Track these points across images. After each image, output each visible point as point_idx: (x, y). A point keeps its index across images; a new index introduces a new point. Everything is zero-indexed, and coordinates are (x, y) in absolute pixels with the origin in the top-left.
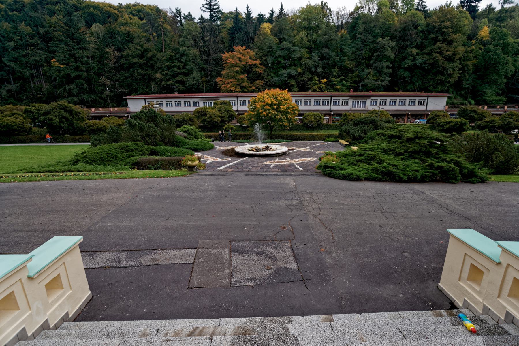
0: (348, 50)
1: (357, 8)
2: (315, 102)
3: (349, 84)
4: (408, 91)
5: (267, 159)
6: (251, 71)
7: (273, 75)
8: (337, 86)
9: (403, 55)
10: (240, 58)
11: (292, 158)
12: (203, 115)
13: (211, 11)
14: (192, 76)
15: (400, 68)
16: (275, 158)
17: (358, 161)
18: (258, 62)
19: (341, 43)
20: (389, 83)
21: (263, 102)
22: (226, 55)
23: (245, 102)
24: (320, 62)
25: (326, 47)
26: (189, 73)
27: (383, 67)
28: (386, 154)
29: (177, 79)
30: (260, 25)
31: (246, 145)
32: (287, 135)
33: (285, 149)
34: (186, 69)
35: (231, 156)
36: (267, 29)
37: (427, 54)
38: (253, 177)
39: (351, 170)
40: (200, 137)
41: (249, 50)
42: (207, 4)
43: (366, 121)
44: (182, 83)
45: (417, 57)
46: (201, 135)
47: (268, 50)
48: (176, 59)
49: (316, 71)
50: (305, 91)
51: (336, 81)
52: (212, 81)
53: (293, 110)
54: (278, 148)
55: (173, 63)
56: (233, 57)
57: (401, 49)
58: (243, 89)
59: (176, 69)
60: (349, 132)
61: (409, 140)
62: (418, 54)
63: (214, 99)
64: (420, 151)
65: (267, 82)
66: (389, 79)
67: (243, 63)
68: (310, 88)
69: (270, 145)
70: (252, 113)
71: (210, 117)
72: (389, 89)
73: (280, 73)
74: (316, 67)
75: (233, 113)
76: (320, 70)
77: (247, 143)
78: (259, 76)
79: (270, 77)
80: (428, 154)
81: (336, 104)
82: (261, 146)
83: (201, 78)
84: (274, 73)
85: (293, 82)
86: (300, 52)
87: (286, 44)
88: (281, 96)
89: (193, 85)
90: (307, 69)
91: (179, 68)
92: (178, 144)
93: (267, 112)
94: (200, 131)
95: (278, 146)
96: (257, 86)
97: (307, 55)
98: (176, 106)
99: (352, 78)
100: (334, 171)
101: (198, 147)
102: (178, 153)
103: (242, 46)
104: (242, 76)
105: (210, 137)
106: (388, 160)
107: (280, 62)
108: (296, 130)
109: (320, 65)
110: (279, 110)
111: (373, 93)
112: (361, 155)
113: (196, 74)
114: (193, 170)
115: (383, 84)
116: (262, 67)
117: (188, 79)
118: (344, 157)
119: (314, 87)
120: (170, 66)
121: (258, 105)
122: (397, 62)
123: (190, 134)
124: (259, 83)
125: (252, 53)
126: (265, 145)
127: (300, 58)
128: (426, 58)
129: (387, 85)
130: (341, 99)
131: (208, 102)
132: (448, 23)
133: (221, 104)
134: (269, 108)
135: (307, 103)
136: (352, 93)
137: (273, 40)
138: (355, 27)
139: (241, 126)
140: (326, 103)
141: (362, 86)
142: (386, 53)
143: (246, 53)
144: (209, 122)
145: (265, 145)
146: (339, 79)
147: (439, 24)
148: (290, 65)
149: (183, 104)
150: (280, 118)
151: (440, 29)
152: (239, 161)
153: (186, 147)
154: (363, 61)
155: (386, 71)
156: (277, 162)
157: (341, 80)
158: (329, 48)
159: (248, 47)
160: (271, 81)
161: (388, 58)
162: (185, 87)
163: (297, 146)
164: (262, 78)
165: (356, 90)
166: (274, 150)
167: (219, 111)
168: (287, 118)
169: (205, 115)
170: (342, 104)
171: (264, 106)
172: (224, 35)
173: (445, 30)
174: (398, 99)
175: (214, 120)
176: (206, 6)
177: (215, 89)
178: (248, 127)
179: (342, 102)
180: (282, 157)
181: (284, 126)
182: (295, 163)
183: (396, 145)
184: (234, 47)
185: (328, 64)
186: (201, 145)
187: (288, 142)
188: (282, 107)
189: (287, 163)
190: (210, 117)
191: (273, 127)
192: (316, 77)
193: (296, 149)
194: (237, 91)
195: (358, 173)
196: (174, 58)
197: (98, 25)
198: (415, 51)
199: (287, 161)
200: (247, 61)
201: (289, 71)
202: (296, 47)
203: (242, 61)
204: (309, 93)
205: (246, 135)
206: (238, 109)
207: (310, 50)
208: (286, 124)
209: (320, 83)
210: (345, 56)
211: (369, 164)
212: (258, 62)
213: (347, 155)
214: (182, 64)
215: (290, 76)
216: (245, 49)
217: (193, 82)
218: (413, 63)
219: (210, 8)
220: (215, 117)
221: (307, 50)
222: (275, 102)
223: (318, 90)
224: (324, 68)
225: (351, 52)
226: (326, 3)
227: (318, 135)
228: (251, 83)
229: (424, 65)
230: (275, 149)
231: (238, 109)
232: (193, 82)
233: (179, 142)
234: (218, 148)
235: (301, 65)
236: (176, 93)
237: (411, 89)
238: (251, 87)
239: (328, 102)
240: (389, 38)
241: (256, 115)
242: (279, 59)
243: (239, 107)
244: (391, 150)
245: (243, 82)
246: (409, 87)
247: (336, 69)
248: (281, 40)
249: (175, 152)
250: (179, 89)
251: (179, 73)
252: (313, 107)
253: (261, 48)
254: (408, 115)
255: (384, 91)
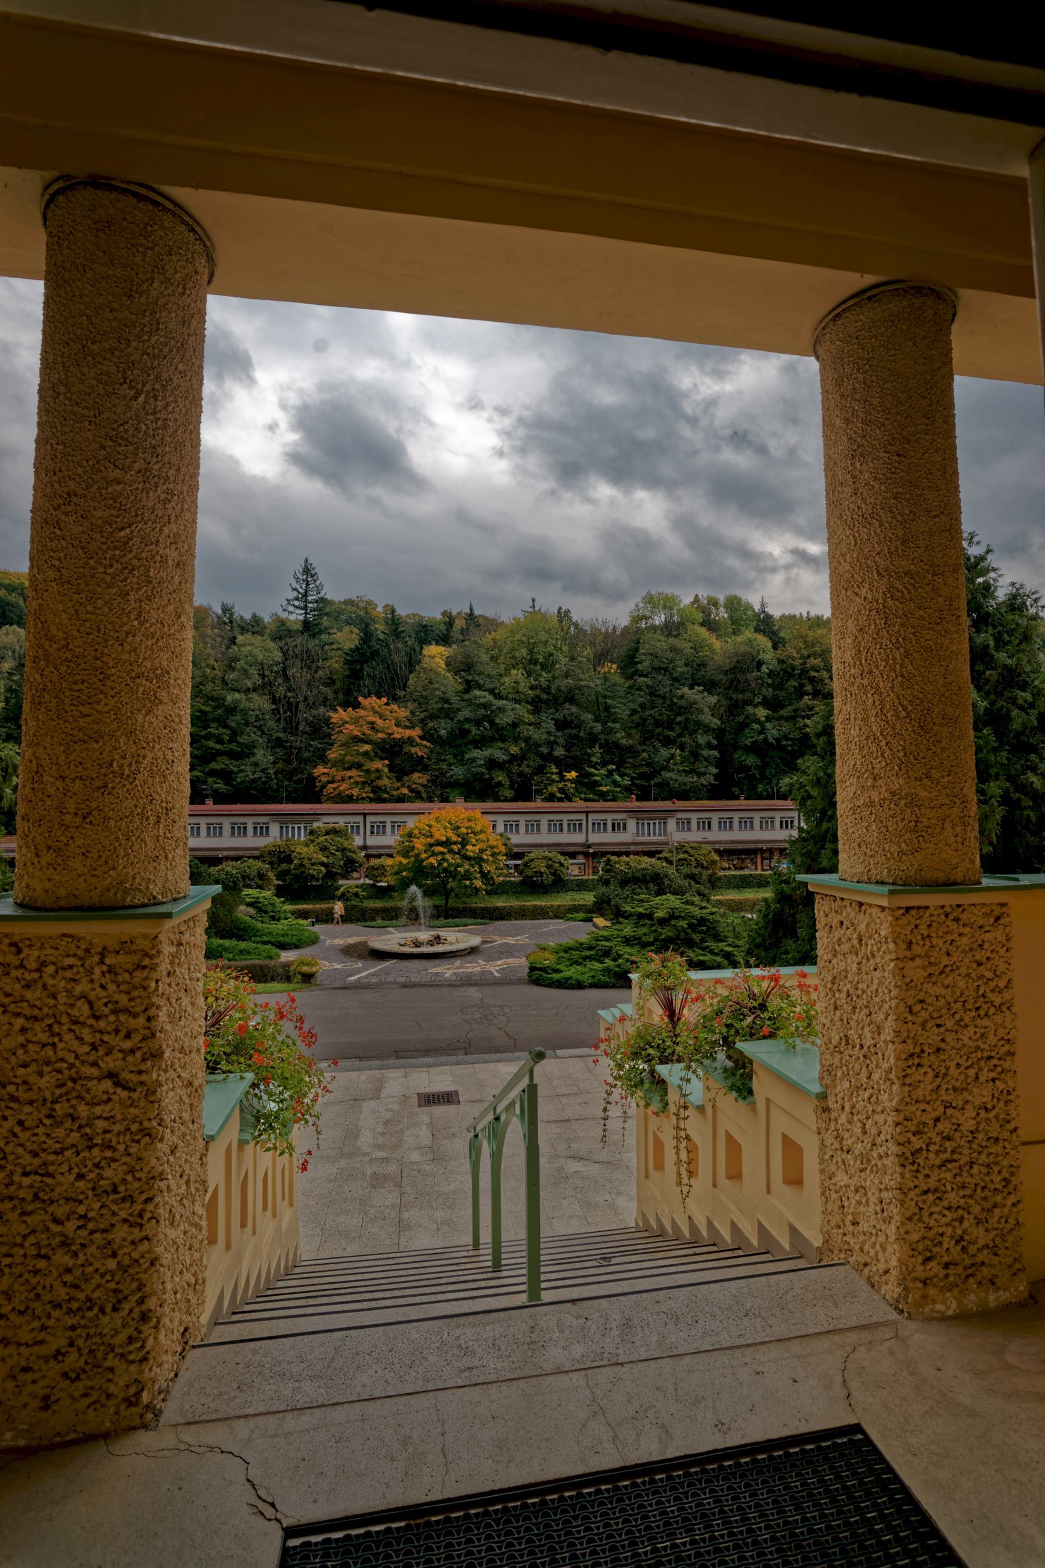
0: (622, 711)
1: (637, 619)
2: (549, 825)
3: (627, 782)
4: (760, 797)
5: (437, 962)
6: (400, 752)
7: (450, 758)
8: (601, 785)
9: (741, 718)
10: (372, 723)
11: (489, 959)
12: (281, 861)
13: (306, 614)
14: (252, 759)
15: (736, 747)
16: (453, 960)
17: (585, 958)
18: (416, 733)
19: (606, 693)
20: (715, 780)
21: (428, 837)
22: (340, 715)
23: (384, 827)
24: (559, 734)
25: (572, 700)
26: (243, 753)
27: (698, 746)
28: (628, 945)
29: (214, 765)
30: (422, 648)
31: (392, 933)
32: (483, 909)
33: (475, 941)
34: (237, 742)
35: (361, 957)
36: (437, 660)
37: (787, 719)
38: (414, 989)
39: (572, 972)
40: (282, 915)
41: (395, 707)
42: (297, 599)
43: (644, 876)
44: (225, 775)
45: (768, 725)
46: (285, 912)
47: (440, 706)
48: (214, 720)
49: (550, 754)
50: (527, 798)
51: (598, 774)
52: (302, 772)
53: (493, 855)
54: (456, 938)
55: (205, 728)
56: (356, 721)
57: (735, 708)
58: (379, 795)
59: (211, 744)
60: (610, 900)
61: (662, 922)
62: (768, 719)
63: (308, 818)
64: (678, 938)
65: (437, 777)
66: (715, 771)
67: (381, 735)
68: (539, 792)
69: (443, 933)
70: (405, 861)
71: (302, 865)
72: (722, 790)
73: (467, 756)
74: (551, 744)
75: (354, 856)
76: (559, 752)
77: (391, 929)
78: (419, 764)
79: (444, 766)
80: (690, 944)
81: (599, 829)
82: (424, 935)
83: (274, 763)
84: (455, 756)
85: (500, 777)
86: (511, 712)
87: (480, 695)
88: (467, 824)
89: (254, 781)
90: (532, 745)
91: (220, 741)
92: (241, 933)
93: (440, 858)
94: (283, 902)
95: (460, 935)
96: (414, 786)
97: (531, 718)
98: (208, 834)
99: (635, 767)
100: (545, 975)
101: (287, 940)
102: (249, 953)
103: (379, 698)
104: (378, 764)
105: (303, 915)
106: (629, 954)
107: (469, 731)
108: (507, 893)
109: (561, 741)
110: (463, 852)
111: (680, 804)
112: (590, 948)
113: (263, 756)
114: (309, 982)
115: (703, 781)
116: (425, 742)
117: (242, 768)
118: (566, 951)
119: (550, 788)
120: (198, 735)
121: (419, 844)
122: (730, 733)
123: (261, 911)
124: (418, 778)
125: (403, 713)
126: (434, 933)
127: (515, 725)
128: (786, 727)
129: (710, 784)
130: (609, 818)
131: (290, 826)
132: (816, 661)
133: (327, 833)
134: (441, 849)
135: (534, 828)
136: (634, 804)
137: (451, 684)
138: (633, 657)
139: (373, 886)
140: (575, 827)
141: (657, 785)
142: (701, 717)
143: (388, 713)
144: (296, 877)
145: (434, 933)
146: (603, 771)
147: (801, 661)
148: (492, 739)
149: (227, 829)
150: (467, 871)
151: (804, 672)
152: (379, 967)
153: (258, 939)
154: (658, 730)
155: (705, 753)
156: (458, 968)
157: (610, 773)
158: (577, 704)
159: (394, 698)
160: (448, 775)
161: (707, 729)
162: (231, 785)
163: (503, 934)
164: (425, 769)
165: (643, 797)
166: (451, 943)
167: (321, 850)
168: (481, 872)
169: (288, 859)
170: (614, 829)
171: (431, 845)
172: (335, 665)
173: (813, 674)
174: (736, 817)
175: (311, 871)
176: (296, 603)
177: (310, 792)
178: (390, 888)
179: (613, 824)
180: (469, 958)
181: (476, 888)
182: (492, 969)
183: (643, 930)
184: (361, 699)
185: (577, 737)
186: (293, 935)
187: (484, 924)
188: (469, 847)
189: (478, 969)
190: (302, 865)
191: (452, 890)
192: (553, 766)
193: (499, 940)
194: (363, 798)
195: (579, 977)
196: (210, 716)
197: (14, 631)
198: (762, 713)
199: (474, 967)
200: (390, 731)
201: (487, 752)
202: (504, 702)
203: (378, 731)
204: (538, 804)
205: (388, 909)
206: (365, 843)
207: (537, 705)
208: (478, 883)
209: (562, 778)
210: (614, 721)
211: (602, 962)
212: (416, 733)
213: (570, 948)
214: (228, 732)
215: (492, 764)
216: (387, 704)
217: (254, 773)
218: (762, 737)
219: (306, 608)
220: (313, 864)
221: (530, 707)
222: (454, 838)
223: (559, 795)
224: (568, 747)
225: (628, 712)
226: (568, 612)
227: (552, 906)
228: (399, 779)
229: (784, 743)
230: (454, 941)
231: (365, 843)
232: (254, 773)
233: (244, 930)
234: (328, 942)
235: (516, 740)
236: (209, 802)
237: (765, 793)
238: (398, 789)
239: (580, 825)
240: (701, 688)
241: (414, 865)
242: (467, 726)
243: (368, 838)
244: (636, 939)
245: (379, 778)
246: (760, 788)
247: (597, 749)
248: (469, 686)
249: (241, 951)
250: (216, 791)
251: (219, 753)
252: (545, 837)
253: (422, 701)
254: (762, 851)
255: (709, 799)
